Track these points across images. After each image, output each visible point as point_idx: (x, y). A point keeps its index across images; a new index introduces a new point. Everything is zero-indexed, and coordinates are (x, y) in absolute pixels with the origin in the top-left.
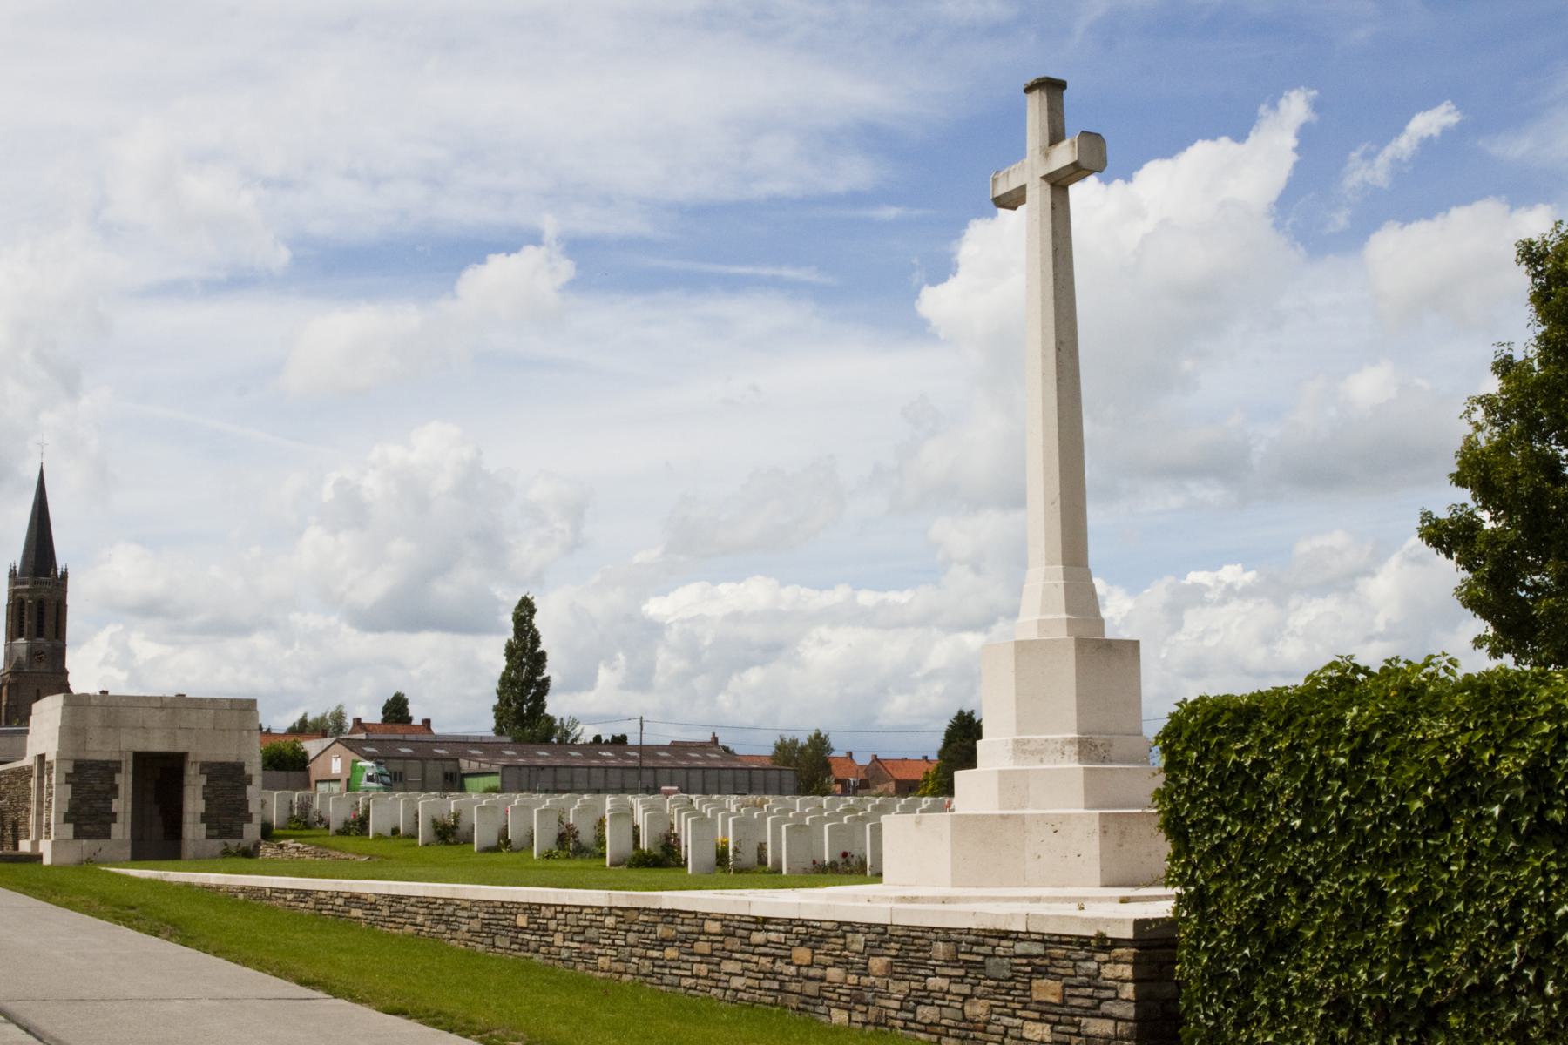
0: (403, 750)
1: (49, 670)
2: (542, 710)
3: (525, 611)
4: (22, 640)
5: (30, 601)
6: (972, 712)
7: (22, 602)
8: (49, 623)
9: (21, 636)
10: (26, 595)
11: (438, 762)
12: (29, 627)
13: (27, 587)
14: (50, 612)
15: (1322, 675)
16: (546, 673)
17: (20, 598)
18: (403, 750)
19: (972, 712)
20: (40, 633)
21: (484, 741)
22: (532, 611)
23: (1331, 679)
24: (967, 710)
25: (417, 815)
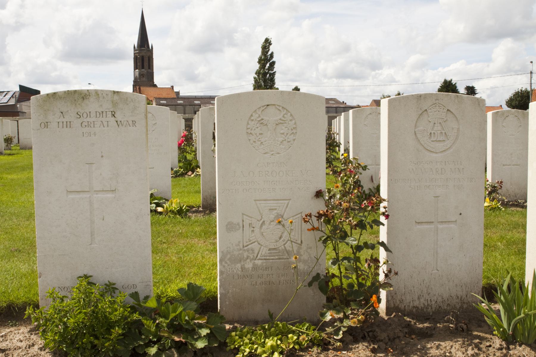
0: (179, 102)
1: (146, 80)
2: (274, 86)
3: (267, 43)
4: (137, 70)
5: (139, 57)
6: (451, 80)
7: (137, 57)
8: (146, 64)
9: (137, 69)
10: (137, 55)
11: (191, 107)
12: (139, 65)
13: (138, 52)
14: (146, 60)
15: (373, 270)
16: (275, 70)
17: (136, 56)
18: (179, 102)
19: (451, 80)
20: (143, 68)
21: (196, 97)
22: (270, 44)
23: (269, 339)
24: (448, 79)
25: (215, 123)
